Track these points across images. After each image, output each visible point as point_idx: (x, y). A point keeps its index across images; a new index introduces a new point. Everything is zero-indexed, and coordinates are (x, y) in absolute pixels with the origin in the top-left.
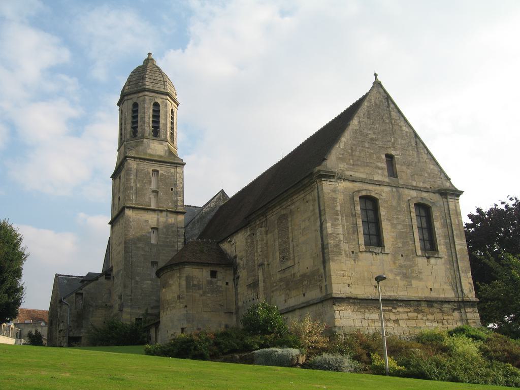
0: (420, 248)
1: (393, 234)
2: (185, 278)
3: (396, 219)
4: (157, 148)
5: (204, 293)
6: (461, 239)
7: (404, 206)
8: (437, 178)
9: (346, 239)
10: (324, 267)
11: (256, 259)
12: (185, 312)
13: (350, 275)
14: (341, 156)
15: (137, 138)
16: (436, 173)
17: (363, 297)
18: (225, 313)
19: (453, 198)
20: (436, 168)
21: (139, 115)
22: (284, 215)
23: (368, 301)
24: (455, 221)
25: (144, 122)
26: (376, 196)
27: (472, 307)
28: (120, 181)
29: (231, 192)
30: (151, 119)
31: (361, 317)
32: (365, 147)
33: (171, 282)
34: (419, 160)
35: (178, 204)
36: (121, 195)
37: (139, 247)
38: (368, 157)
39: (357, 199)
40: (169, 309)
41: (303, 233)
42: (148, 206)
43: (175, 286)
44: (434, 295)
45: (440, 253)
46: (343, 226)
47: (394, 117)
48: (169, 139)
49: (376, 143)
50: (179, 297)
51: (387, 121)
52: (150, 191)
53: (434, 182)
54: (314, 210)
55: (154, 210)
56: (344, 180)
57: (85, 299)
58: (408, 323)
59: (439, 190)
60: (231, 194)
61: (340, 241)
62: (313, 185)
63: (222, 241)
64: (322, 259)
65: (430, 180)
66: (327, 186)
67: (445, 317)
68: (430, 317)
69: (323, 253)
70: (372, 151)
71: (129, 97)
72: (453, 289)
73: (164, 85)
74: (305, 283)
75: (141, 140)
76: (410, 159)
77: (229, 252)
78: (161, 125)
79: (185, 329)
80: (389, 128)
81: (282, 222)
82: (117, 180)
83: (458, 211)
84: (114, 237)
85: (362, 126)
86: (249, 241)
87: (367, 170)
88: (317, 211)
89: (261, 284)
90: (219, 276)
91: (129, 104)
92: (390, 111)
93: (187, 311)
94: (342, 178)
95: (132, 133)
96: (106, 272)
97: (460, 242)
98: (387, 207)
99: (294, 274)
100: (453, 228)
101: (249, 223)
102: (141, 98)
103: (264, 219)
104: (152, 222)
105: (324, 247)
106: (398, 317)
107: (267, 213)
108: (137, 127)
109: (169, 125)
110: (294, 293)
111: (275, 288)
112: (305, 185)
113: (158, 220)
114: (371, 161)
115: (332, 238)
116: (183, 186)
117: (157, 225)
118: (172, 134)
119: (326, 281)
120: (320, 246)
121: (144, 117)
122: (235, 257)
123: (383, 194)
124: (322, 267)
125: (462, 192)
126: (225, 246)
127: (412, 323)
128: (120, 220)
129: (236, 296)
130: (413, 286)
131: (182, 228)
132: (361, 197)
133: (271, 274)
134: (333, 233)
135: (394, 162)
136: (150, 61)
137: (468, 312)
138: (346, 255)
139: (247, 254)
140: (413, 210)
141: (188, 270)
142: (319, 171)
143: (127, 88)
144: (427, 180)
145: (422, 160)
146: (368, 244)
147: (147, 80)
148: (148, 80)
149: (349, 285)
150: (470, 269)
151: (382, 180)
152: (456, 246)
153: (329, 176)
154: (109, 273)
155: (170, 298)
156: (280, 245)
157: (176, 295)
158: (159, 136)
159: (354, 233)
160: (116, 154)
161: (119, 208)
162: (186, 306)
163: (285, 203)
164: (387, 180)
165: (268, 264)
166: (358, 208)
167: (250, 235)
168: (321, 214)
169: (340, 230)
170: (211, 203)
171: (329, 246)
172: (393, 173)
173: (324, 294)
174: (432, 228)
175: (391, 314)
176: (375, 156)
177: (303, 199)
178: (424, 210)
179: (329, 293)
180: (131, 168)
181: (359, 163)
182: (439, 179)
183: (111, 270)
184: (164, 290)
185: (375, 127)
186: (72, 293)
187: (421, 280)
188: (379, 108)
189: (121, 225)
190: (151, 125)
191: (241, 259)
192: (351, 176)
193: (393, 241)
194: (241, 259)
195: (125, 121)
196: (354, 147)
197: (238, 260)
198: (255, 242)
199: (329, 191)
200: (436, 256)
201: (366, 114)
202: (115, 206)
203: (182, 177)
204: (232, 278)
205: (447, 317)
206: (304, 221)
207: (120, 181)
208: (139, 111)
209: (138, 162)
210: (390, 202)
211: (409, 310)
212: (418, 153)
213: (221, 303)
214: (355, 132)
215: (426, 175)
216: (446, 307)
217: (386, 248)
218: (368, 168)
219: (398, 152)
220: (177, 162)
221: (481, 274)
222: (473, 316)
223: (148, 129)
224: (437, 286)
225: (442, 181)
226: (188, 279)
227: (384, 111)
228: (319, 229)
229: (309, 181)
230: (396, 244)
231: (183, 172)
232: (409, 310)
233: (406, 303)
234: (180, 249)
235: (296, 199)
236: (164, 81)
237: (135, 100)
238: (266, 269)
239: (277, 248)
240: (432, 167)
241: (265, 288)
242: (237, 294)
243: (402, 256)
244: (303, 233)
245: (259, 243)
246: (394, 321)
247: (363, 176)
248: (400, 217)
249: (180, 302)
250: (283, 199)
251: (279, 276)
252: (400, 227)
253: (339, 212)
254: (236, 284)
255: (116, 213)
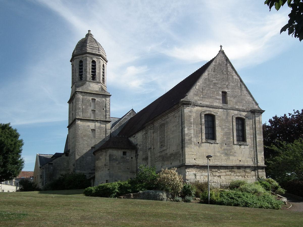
0: (236, 140)
1: (221, 133)
2: (108, 156)
3: (224, 126)
4: (94, 87)
5: (119, 163)
6: (260, 135)
7: (230, 119)
8: (250, 103)
9: (195, 136)
10: (182, 150)
11: (148, 145)
12: (109, 172)
13: (196, 154)
14: (196, 93)
15: (82, 81)
16: (250, 101)
17: (202, 165)
18: (130, 172)
19: (258, 114)
20: (251, 98)
21: (83, 68)
22: (163, 124)
23: (205, 167)
24: (258, 126)
25: (86, 72)
26: (214, 114)
27: (262, 169)
28: (73, 105)
29: (137, 110)
30: (91, 70)
31: (200, 174)
32: (210, 88)
33: (101, 157)
34: (241, 94)
35: (107, 117)
36: (74, 112)
37: (84, 140)
38: (211, 93)
39: (203, 115)
40: (100, 171)
41: (172, 133)
42: (90, 118)
43: (103, 159)
44: (241, 164)
45: (247, 143)
46: (194, 129)
47: (230, 71)
48: (102, 82)
49: (217, 85)
50: (105, 165)
51: (225, 73)
52: (91, 110)
53: (249, 106)
54: (179, 121)
55: (93, 120)
56: (197, 106)
57: (54, 166)
58: (225, 177)
59: (251, 110)
60: (137, 111)
61: (191, 138)
62: (179, 108)
63: (130, 137)
64: (181, 146)
65: (246, 105)
66: (187, 110)
67: (246, 174)
68: (238, 174)
69: (182, 143)
70: (214, 90)
71: (77, 57)
72: (253, 161)
73: (98, 50)
74: (172, 158)
75: (85, 82)
76: (236, 93)
77: (133, 142)
78: (97, 74)
79: (108, 181)
80: (226, 77)
81: (162, 127)
82: (71, 104)
83: (261, 121)
84: (70, 134)
85: (210, 76)
86: (144, 137)
87: (210, 100)
88: (180, 122)
89: (149, 159)
90: (128, 154)
91: (77, 61)
92: (227, 67)
93: (109, 172)
94: (195, 105)
95: (79, 78)
96: (66, 152)
97: (260, 137)
98: (220, 120)
99: (167, 153)
100: (256, 130)
101: (145, 128)
102: (85, 58)
103: (153, 126)
104: (92, 127)
105: (183, 141)
106: (220, 174)
107: (154, 122)
108: (82, 75)
109: (102, 74)
110: (166, 163)
111: (157, 160)
112: (174, 108)
113: (95, 125)
114: (213, 96)
115: (187, 136)
116: (110, 107)
117: (95, 128)
118: (103, 79)
119: (183, 157)
120: (181, 140)
121: (87, 69)
122: (137, 145)
123: (219, 113)
124: (181, 150)
125: (264, 111)
126: (132, 139)
127: (228, 177)
128: (74, 125)
129: (136, 164)
130: (230, 159)
131: (109, 129)
132: (205, 115)
133: (155, 153)
134: (188, 133)
135: (226, 96)
136: (89, 35)
137: (259, 172)
138: (195, 144)
139: (143, 143)
140: (234, 121)
141: (110, 151)
142: (183, 101)
143: (75, 51)
144: (245, 105)
145: (243, 94)
146: (207, 138)
147: (88, 47)
148: (89, 47)
149: (195, 159)
150: (263, 151)
151: (218, 105)
152: (257, 139)
153: (188, 104)
154: (67, 153)
155: (100, 165)
156: (160, 139)
157: (103, 164)
158: (96, 80)
159: (200, 133)
160: (70, 90)
161: (72, 119)
162: (109, 170)
163: (164, 117)
164: (221, 105)
165: (154, 149)
166: (203, 120)
167: (145, 134)
168: (182, 123)
169: (192, 131)
170: (126, 116)
171: (185, 140)
172: (225, 101)
173: (181, 164)
174: (244, 130)
175: (216, 173)
176: (216, 93)
177: (174, 116)
178: (241, 122)
179: (184, 163)
180: (79, 98)
181: (206, 96)
182: (251, 104)
183: (69, 151)
184: (97, 162)
185: (218, 77)
186: (46, 163)
187: (235, 156)
188: (221, 65)
189: (74, 128)
190: (91, 73)
191: (140, 146)
192: (201, 103)
193: (221, 137)
194: (140, 146)
195: (75, 71)
196: (204, 88)
197: (138, 146)
198: (147, 137)
199: (188, 112)
200: (245, 144)
201: (213, 70)
202: (71, 118)
203: (109, 103)
204: (135, 155)
205: (248, 174)
206: (173, 127)
207: (73, 105)
208: (83, 65)
209: (83, 94)
210: (222, 117)
211: (227, 171)
212: (241, 90)
213: (128, 168)
214: (206, 79)
215: (244, 102)
216: (248, 170)
217: (217, 140)
218: (211, 99)
219: (229, 90)
220: (106, 94)
221: (268, 153)
222: (262, 174)
223: (89, 76)
224: (243, 159)
225: (253, 105)
226: (110, 156)
227: (224, 67)
228: (181, 131)
229: (177, 107)
230: (223, 138)
231: (110, 100)
232: (227, 171)
233: (226, 167)
234: (108, 140)
235: (170, 116)
236: (98, 48)
237: (81, 59)
238: (152, 151)
239: (159, 141)
240: (248, 98)
241: (151, 160)
242: (137, 163)
243: (226, 144)
244: (172, 133)
245: (149, 138)
246: (218, 176)
247: (208, 103)
248: (226, 124)
249: (106, 167)
250: (163, 116)
251: (159, 154)
252: (226, 130)
253: (192, 123)
254: (136, 158)
255: (71, 122)
